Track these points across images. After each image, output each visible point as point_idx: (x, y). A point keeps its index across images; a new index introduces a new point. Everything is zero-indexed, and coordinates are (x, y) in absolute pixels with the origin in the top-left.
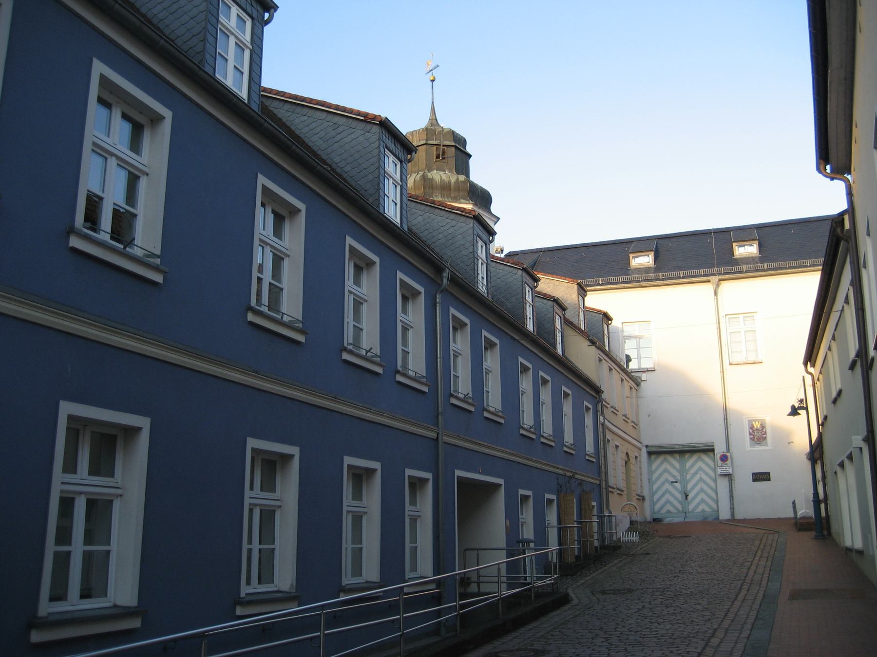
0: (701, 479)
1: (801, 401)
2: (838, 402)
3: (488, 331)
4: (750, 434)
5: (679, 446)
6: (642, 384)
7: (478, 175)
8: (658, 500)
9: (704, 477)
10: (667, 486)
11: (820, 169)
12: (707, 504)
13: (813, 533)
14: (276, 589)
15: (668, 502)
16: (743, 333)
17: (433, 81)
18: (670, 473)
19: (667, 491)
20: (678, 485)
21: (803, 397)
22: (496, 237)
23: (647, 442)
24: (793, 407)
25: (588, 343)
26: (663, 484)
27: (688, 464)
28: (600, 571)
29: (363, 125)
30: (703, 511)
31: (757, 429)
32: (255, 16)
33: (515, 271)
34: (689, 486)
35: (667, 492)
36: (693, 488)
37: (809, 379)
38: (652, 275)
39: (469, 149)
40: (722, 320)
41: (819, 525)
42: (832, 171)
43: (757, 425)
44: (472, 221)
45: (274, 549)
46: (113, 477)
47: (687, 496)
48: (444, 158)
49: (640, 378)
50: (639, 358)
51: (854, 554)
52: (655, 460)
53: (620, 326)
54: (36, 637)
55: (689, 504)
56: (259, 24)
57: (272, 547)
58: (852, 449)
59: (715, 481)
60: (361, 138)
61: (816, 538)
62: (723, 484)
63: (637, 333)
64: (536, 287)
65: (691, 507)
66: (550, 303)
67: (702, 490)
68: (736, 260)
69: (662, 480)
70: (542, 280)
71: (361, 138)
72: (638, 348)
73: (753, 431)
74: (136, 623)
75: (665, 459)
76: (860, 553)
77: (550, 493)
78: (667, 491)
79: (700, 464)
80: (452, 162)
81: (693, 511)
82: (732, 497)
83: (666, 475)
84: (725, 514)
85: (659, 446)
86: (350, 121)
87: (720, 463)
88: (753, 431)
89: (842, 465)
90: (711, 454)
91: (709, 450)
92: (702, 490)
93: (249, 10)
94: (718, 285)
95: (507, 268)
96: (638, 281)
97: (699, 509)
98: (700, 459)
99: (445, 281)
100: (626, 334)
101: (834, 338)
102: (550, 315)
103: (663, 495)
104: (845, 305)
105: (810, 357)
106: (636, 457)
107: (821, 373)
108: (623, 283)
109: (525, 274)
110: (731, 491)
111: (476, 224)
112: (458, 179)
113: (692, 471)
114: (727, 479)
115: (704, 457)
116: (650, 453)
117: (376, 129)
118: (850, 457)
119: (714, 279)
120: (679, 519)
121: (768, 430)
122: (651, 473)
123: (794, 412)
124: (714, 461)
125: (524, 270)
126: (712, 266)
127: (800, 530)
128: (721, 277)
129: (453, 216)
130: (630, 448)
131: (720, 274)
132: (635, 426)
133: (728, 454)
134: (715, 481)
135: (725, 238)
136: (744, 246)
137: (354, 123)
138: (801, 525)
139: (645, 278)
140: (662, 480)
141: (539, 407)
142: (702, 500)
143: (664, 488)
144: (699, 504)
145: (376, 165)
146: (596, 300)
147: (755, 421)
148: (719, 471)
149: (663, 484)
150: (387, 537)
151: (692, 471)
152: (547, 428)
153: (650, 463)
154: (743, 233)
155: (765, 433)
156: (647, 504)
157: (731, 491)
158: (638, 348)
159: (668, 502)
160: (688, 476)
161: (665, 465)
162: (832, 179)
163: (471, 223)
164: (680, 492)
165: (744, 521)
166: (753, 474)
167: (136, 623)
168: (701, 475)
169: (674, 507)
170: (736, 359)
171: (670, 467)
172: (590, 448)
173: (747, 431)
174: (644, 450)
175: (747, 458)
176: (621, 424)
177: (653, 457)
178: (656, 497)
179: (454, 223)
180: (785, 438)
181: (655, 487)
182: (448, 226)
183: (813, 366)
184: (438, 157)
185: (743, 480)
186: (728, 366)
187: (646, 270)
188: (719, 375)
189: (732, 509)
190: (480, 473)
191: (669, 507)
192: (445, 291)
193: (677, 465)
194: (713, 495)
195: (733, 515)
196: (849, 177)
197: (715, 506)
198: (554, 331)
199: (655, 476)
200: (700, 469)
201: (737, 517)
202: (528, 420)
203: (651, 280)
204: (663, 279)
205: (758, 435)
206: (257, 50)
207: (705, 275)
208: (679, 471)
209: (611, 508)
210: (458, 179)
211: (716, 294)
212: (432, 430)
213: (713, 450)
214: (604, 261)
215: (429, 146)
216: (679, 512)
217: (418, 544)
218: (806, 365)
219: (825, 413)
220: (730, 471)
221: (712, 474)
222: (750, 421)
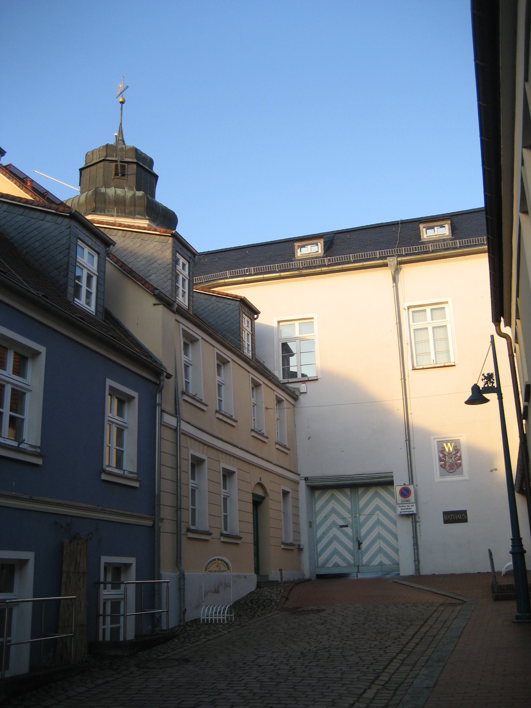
0: (378, 522)
1: (489, 377)
4: (441, 460)
6: (302, 398)
7: (163, 196)
9: (383, 519)
10: (335, 531)
15: (336, 552)
17: (122, 103)
19: (335, 538)
20: (348, 530)
21: (492, 371)
22: (260, 315)
23: (305, 473)
25: (154, 301)
26: (329, 528)
27: (362, 502)
30: (381, 564)
31: (450, 453)
34: (363, 531)
35: (333, 537)
37: (501, 344)
39: (156, 170)
40: (404, 314)
43: (449, 448)
46: (377, 505)
47: (360, 544)
48: (123, 175)
49: (298, 389)
55: (362, 555)
62: (404, 528)
63: (297, 334)
69: (328, 523)
73: (445, 456)
75: (333, 497)
80: (132, 179)
81: (368, 564)
82: (416, 544)
84: (407, 569)
85: (323, 478)
87: (399, 498)
88: (445, 456)
91: (386, 483)
96: (299, 269)
97: (376, 562)
98: (377, 494)
106: (285, 494)
110: (415, 537)
112: (134, 194)
113: (367, 511)
114: (408, 523)
115: (382, 492)
119: (392, 261)
121: (464, 454)
123: (477, 397)
127: (497, 599)
133: (411, 488)
136: (432, 228)
140: (328, 523)
142: (380, 550)
143: (330, 535)
147: (447, 442)
148: (399, 510)
149: (329, 528)
151: (367, 511)
155: (460, 458)
156: (305, 556)
157: (415, 537)
160: (362, 518)
164: (352, 540)
169: (344, 559)
171: (338, 506)
173: (436, 455)
174: (303, 484)
175: (436, 491)
177: (317, 493)
183: (508, 324)
184: (116, 174)
186: (392, 354)
189: (417, 561)
191: (337, 559)
193: (347, 503)
195: (417, 569)
199: (319, 519)
200: (377, 508)
205: (451, 461)
207: (381, 258)
208: (350, 512)
210: (134, 194)
211: (395, 280)
213: (391, 483)
214: (274, 258)
215: (107, 163)
218: (496, 321)
219: (527, 379)
220: (414, 509)
222: (440, 443)
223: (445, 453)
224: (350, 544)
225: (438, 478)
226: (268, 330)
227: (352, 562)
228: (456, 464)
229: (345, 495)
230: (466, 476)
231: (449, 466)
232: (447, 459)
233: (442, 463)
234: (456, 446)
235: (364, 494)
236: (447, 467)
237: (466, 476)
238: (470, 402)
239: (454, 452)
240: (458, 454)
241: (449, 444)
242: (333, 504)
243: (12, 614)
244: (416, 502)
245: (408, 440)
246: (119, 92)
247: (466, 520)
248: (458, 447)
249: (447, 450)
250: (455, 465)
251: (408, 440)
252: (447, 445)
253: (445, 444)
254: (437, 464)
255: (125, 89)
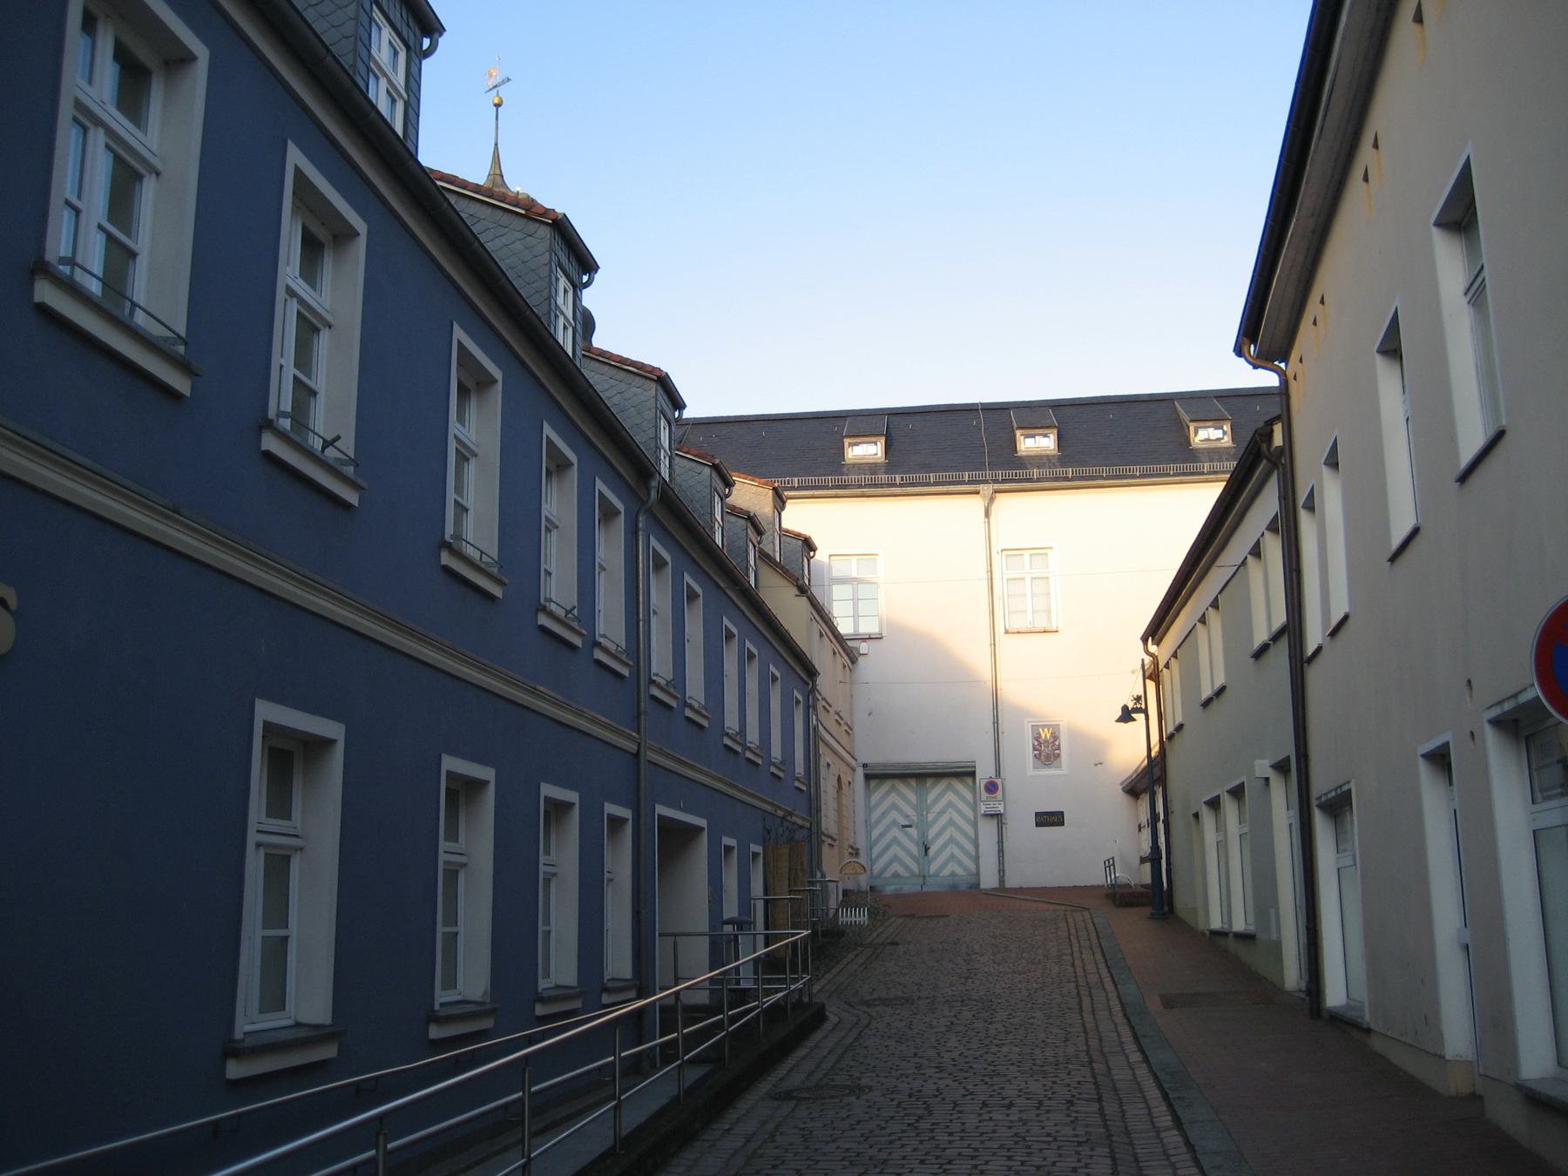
1: (1138, 699)
2: (1214, 705)
3: (692, 576)
5: (919, 766)
6: (860, 659)
8: (880, 855)
10: (895, 832)
11: (1239, 351)
12: (960, 863)
13: (1149, 910)
14: (460, 998)
15: (895, 858)
16: (1028, 580)
17: (498, 106)
18: (900, 811)
19: (895, 840)
20: (913, 831)
24: (1125, 708)
25: (795, 591)
26: (888, 829)
27: (931, 797)
28: (835, 971)
29: (519, 223)
30: (953, 874)
32: (411, 43)
33: (699, 468)
34: (932, 833)
35: (887, 844)
36: (938, 835)
38: (883, 477)
40: (996, 558)
41: (1155, 898)
42: (1259, 356)
43: (1045, 734)
44: (654, 385)
45: (286, 938)
46: (289, 818)
47: (927, 849)
49: (857, 649)
50: (856, 617)
51: (1231, 940)
52: (877, 787)
53: (826, 560)
54: (235, 1070)
56: (416, 56)
57: (282, 933)
58: (1243, 779)
59: (975, 825)
60: (518, 245)
61: (1153, 917)
62: (988, 830)
63: (854, 574)
64: (727, 496)
65: (933, 868)
66: (742, 522)
67: (952, 840)
68: (1020, 458)
69: (886, 822)
70: (737, 486)
71: (518, 245)
72: (855, 600)
74: (329, 1052)
75: (893, 788)
76: (1246, 938)
77: (756, 843)
78: (895, 840)
79: (950, 796)
81: (936, 875)
82: (1001, 851)
83: (894, 814)
85: (885, 765)
86: (500, 213)
87: (984, 795)
89: (1214, 804)
90: (969, 780)
91: (965, 774)
92: (952, 840)
93: (405, 34)
94: (992, 500)
95: (686, 463)
96: (860, 486)
97: (946, 872)
99: (653, 494)
100: (835, 574)
101: (1215, 604)
102: (742, 543)
103: (888, 846)
104: (1250, 559)
105: (1155, 631)
107: (1175, 655)
108: (834, 487)
109: (714, 475)
110: (1001, 842)
111: (660, 390)
113: (937, 809)
114: (993, 823)
115: (957, 784)
116: (868, 777)
117: (545, 232)
118: (1237, 793)
119: (986, 489)
120: (909, 888)
122: (869, 809)
123: (1126, 716)
124: (974, 793)
125: (715, 467)
126: (981, 467)
127: (1121, 905)
128: (997, 486)
129: (622, 375)
130: (844, 768)
131: (996, 481)
132: (849, 732)
133: (999, 781)
134: (975, 825)
135: (1001, 420)
136: (1033, 436)
137: (506, 219)
138: (1120, 897)
139: (869, 482)
140: (886, 822)
141: (747, 704)
143: (888, 837)
144: (945, 865)
145: (546, 293)
146: (801, 516)
147: (1043, 727)
148: (983, 809)
149: (888, 829)
150: (552, 915)
151: (937, 809)
152: (753, 736)
153: (868, 792)
154: (1034, 414)
157: (1001, 842)
158: (855, 600)
159: (895, 858)
161: (894, 798)
162: (1255, 367)
163: (653, 388)
165: (1021, 890)
166: (1037, 814)
167: (329, 1052)
168: (951, 814)
169: (907, 868)
170: (1018, 623)
171: (899, 801)
172: (800, 769)
174: (860, 772)
175: (1029, 786)
176: (833, 727)
177: (873, 783)
178: (875, 852)
179: (623, 386)
180: (1095, 755)
181: (875, 833)
182: (612, 392)
185: (1021, 825)
187: (872, 468)
188: (988, 650)
189: (1001, 871)
190: (680, 809)
191: (896, 867)
192: (649, 512)
193: (912, 797)
194: (970, 847)
195: (1002, 881)
196: (1283, 365)
197: (972, 867)
198: (747, 569)
200: (950, 804)
201: (1008, 885)
202: (731, 722)
203: (882, 486)
204: (901, 485)
205: (1047, 750)
206: (413, 100)
207: (970, 482)
208: (915, 809)
209: (825, 868)
211: (987, 514)
212: (629, 737)
213: (973, 774)
214: (805, 448)
216: (913, 875)
217: (461, 928)
218: (1145, 640)
220: (1001, 808)
221: (970, 814)
224: (914, 850)
225: (1030, 771)
226: (821, 563)
227: (916, 871)
229: (908, 785)
230: (1065, 770)
235: (934, 785)
237: (1065, 770)
238: (1121, 720)
242: (893, 797)
244: (1004, 799)
245: (996, 723)
246: (491, 84)
247: (1062, 824)
251: (996, 723)
254: (1030, 753)
255: (503, 82)
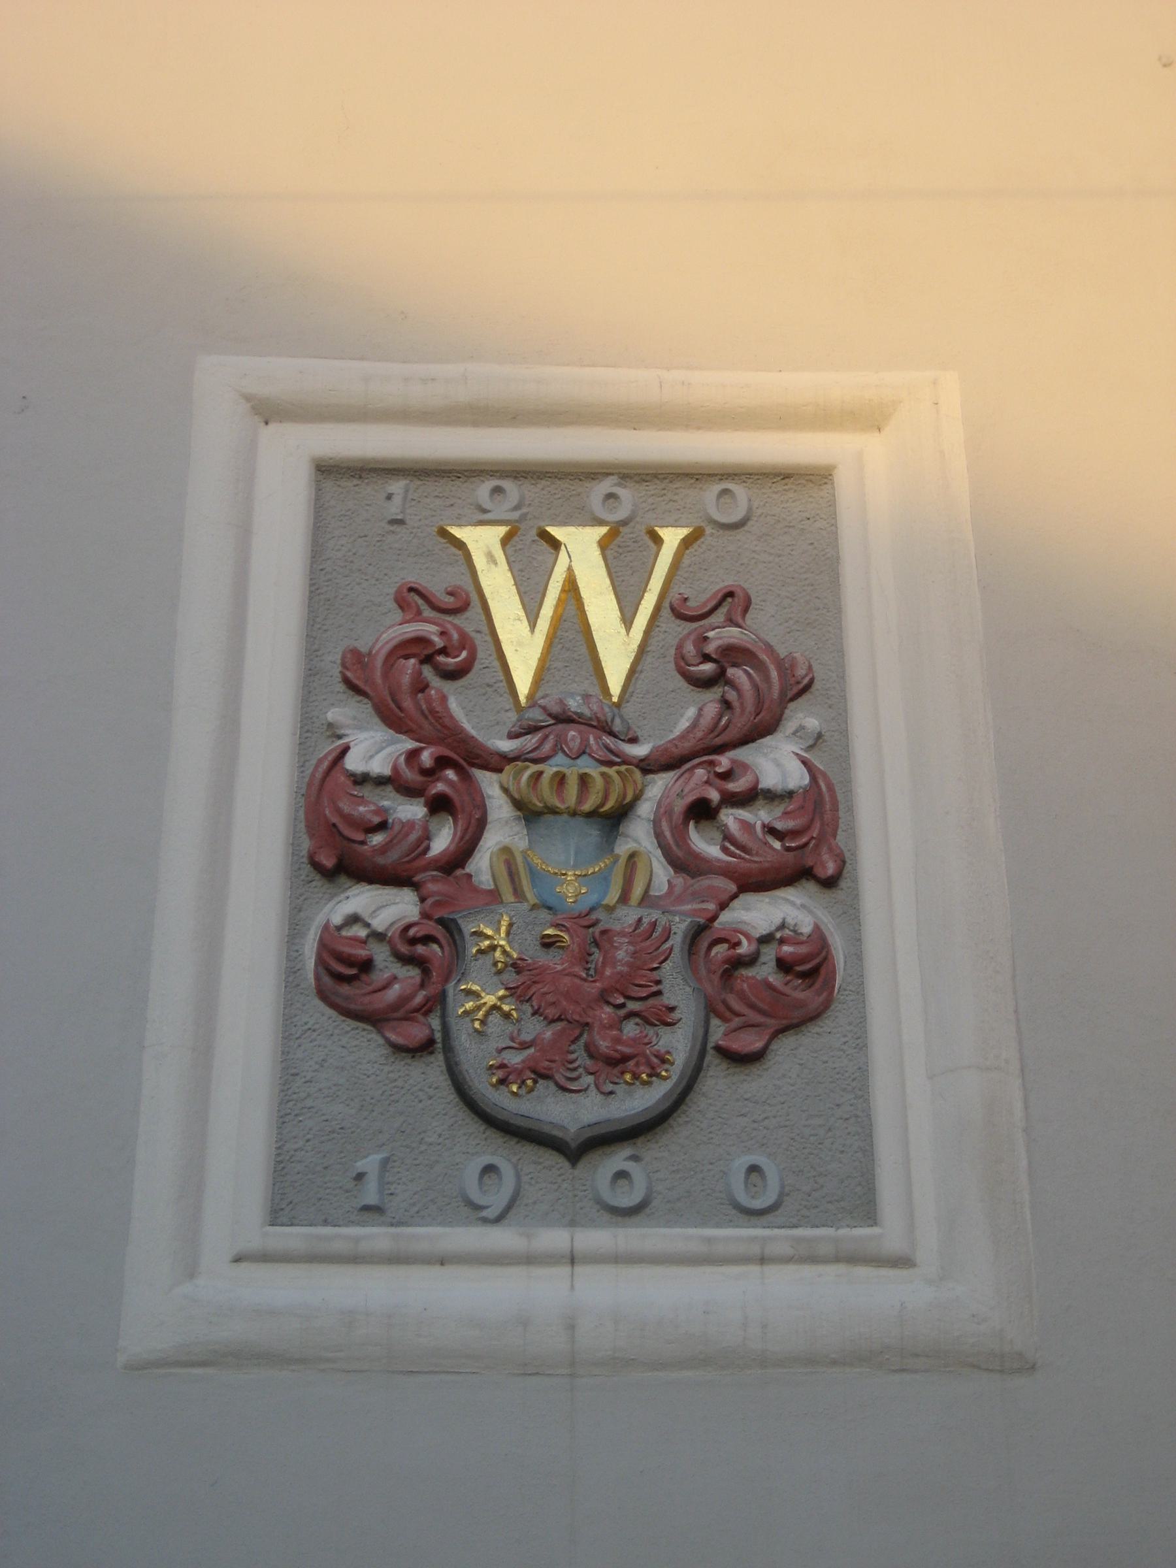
4: (338, 850)
31: (568, 720)
43: (562, 617)
88: (448, 767)
121: (907, 760)
155: (810, 849)
223: (461, 706)
228: (725, 966)
230: (937, 1249)
231: (523, 980)
232: (502, 831)
233: (391, 908)
234: (733, 603)
236: (481, 993)
237: (937, 1249)
239: (686, 714)
240: (777, 763)
241: (581, 549)
243: (639, 1124)
248: (766, 626)
249: (522, 649)
250: (679, 991)
252: (531, 550)
253: (482, 540)
254: (232, 913)
